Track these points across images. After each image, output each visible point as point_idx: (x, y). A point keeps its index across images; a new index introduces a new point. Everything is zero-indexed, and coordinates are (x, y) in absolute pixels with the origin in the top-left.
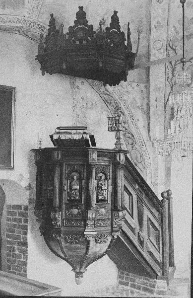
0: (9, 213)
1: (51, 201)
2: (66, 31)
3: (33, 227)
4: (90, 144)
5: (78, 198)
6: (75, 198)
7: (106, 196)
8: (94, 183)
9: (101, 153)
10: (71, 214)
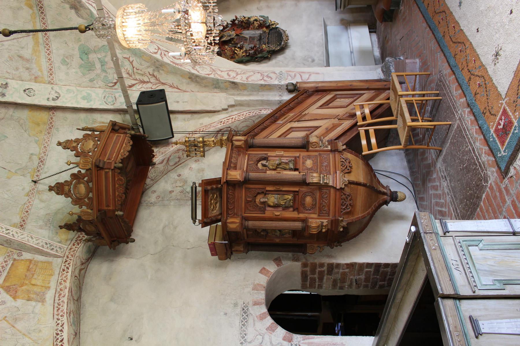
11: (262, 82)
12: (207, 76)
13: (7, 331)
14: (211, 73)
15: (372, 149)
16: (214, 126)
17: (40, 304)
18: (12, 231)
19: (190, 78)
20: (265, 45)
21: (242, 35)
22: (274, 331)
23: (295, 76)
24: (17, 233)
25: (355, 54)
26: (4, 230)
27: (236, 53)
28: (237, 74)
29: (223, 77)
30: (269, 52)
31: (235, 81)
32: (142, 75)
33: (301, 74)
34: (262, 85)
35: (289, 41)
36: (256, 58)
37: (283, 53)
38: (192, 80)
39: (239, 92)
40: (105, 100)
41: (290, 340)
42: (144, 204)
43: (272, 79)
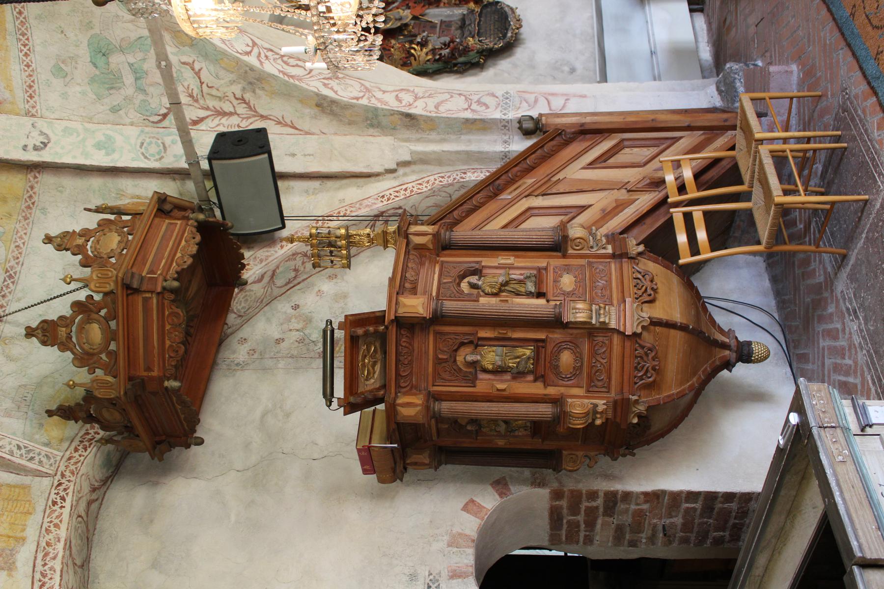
0: (572, 538)
1: (537, 427)
2: (83, 376)
3: (608, 477)
4: (693, 505)
5: (528, 352)
6: (529, 358)
7: (527, 272)
8: (487, 304)
9: (401, 285)
10: (577, 371)
11: (468, 115)
12: (355, 101)
14: (362, 94)
19: (318, 105)
20: (473, 37)
21: (426, 18)
23: (536, 101)
25: (661, 57)
27: (413, 55)
28: (416, 98)
29: (386, 103)
30: (481, 52)
31: (412, 111)
32: (220, 99)
33: (550, 98)
34: (467, 121)
35: (522, 30)
36: (455, 65)
37: (510, 56)
38: (323, 111)
39: (418, 136)
40: (143, 150)
42: (222, 366)
43: (487, 107)
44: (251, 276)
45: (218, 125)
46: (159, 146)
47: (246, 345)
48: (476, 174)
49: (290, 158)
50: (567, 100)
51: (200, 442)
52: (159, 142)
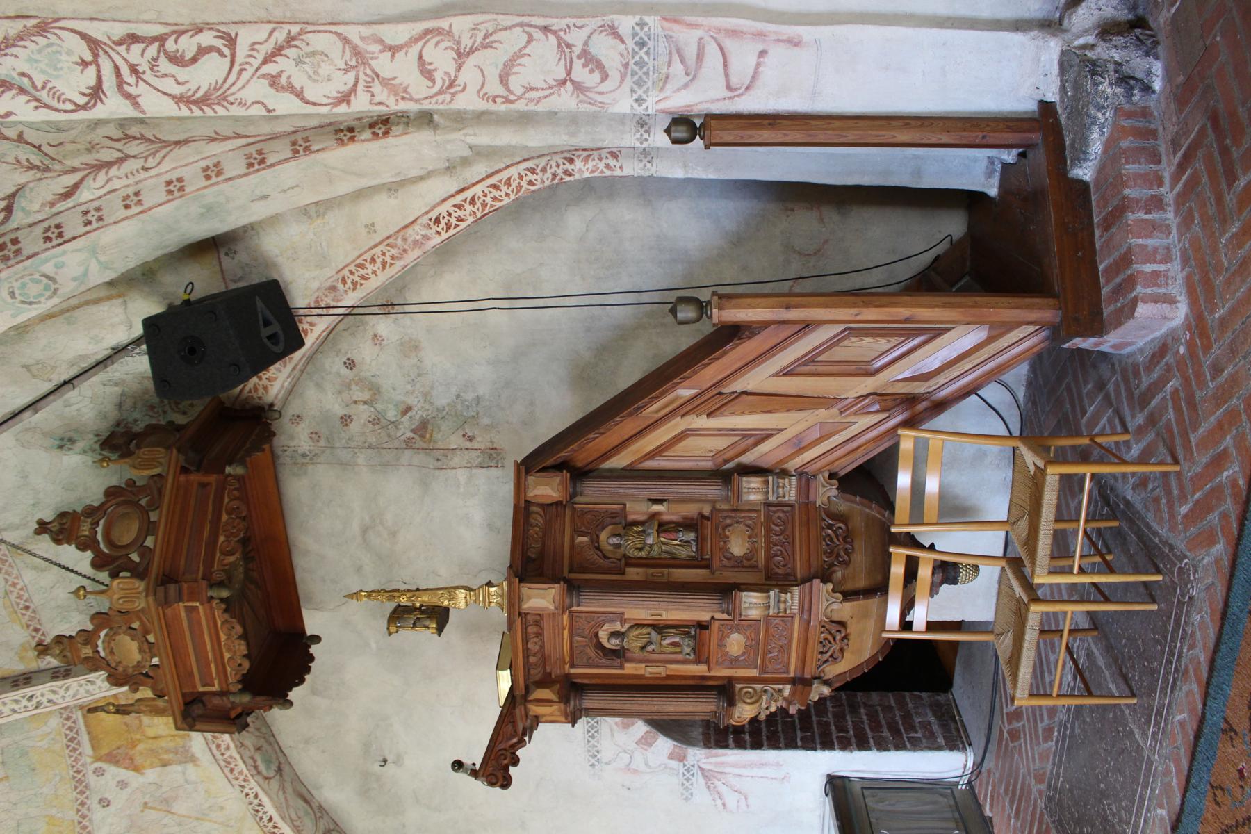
12: (343, 108)
13: (164, 822)
15: (909, 558)
16: (416, 243)
17: (190, 766)
18: (42, 695)
22: (650, 745)
24: (54, 692)
26: (24, 702)
32: (89, 151)
33: (728, 43)
40: (20, 298)
41: (682, 759)
42: (285, 459)
44: (280, 391)
45: (107, 182)
46: (39, 282)
47: (302, 425)
48: (591, 164)
49: (262, 203)
50: (762, 53)
51: (316, 639)
52: (37, 276)
